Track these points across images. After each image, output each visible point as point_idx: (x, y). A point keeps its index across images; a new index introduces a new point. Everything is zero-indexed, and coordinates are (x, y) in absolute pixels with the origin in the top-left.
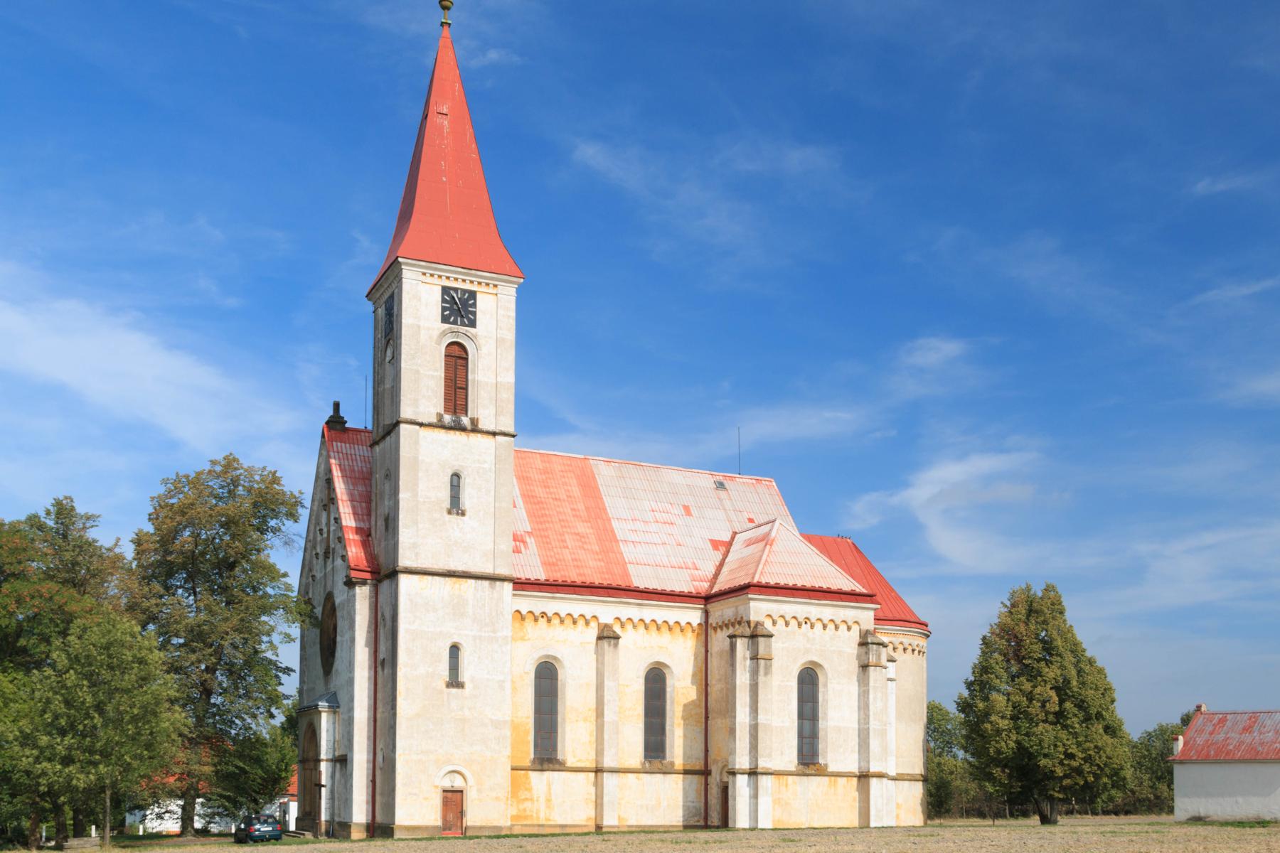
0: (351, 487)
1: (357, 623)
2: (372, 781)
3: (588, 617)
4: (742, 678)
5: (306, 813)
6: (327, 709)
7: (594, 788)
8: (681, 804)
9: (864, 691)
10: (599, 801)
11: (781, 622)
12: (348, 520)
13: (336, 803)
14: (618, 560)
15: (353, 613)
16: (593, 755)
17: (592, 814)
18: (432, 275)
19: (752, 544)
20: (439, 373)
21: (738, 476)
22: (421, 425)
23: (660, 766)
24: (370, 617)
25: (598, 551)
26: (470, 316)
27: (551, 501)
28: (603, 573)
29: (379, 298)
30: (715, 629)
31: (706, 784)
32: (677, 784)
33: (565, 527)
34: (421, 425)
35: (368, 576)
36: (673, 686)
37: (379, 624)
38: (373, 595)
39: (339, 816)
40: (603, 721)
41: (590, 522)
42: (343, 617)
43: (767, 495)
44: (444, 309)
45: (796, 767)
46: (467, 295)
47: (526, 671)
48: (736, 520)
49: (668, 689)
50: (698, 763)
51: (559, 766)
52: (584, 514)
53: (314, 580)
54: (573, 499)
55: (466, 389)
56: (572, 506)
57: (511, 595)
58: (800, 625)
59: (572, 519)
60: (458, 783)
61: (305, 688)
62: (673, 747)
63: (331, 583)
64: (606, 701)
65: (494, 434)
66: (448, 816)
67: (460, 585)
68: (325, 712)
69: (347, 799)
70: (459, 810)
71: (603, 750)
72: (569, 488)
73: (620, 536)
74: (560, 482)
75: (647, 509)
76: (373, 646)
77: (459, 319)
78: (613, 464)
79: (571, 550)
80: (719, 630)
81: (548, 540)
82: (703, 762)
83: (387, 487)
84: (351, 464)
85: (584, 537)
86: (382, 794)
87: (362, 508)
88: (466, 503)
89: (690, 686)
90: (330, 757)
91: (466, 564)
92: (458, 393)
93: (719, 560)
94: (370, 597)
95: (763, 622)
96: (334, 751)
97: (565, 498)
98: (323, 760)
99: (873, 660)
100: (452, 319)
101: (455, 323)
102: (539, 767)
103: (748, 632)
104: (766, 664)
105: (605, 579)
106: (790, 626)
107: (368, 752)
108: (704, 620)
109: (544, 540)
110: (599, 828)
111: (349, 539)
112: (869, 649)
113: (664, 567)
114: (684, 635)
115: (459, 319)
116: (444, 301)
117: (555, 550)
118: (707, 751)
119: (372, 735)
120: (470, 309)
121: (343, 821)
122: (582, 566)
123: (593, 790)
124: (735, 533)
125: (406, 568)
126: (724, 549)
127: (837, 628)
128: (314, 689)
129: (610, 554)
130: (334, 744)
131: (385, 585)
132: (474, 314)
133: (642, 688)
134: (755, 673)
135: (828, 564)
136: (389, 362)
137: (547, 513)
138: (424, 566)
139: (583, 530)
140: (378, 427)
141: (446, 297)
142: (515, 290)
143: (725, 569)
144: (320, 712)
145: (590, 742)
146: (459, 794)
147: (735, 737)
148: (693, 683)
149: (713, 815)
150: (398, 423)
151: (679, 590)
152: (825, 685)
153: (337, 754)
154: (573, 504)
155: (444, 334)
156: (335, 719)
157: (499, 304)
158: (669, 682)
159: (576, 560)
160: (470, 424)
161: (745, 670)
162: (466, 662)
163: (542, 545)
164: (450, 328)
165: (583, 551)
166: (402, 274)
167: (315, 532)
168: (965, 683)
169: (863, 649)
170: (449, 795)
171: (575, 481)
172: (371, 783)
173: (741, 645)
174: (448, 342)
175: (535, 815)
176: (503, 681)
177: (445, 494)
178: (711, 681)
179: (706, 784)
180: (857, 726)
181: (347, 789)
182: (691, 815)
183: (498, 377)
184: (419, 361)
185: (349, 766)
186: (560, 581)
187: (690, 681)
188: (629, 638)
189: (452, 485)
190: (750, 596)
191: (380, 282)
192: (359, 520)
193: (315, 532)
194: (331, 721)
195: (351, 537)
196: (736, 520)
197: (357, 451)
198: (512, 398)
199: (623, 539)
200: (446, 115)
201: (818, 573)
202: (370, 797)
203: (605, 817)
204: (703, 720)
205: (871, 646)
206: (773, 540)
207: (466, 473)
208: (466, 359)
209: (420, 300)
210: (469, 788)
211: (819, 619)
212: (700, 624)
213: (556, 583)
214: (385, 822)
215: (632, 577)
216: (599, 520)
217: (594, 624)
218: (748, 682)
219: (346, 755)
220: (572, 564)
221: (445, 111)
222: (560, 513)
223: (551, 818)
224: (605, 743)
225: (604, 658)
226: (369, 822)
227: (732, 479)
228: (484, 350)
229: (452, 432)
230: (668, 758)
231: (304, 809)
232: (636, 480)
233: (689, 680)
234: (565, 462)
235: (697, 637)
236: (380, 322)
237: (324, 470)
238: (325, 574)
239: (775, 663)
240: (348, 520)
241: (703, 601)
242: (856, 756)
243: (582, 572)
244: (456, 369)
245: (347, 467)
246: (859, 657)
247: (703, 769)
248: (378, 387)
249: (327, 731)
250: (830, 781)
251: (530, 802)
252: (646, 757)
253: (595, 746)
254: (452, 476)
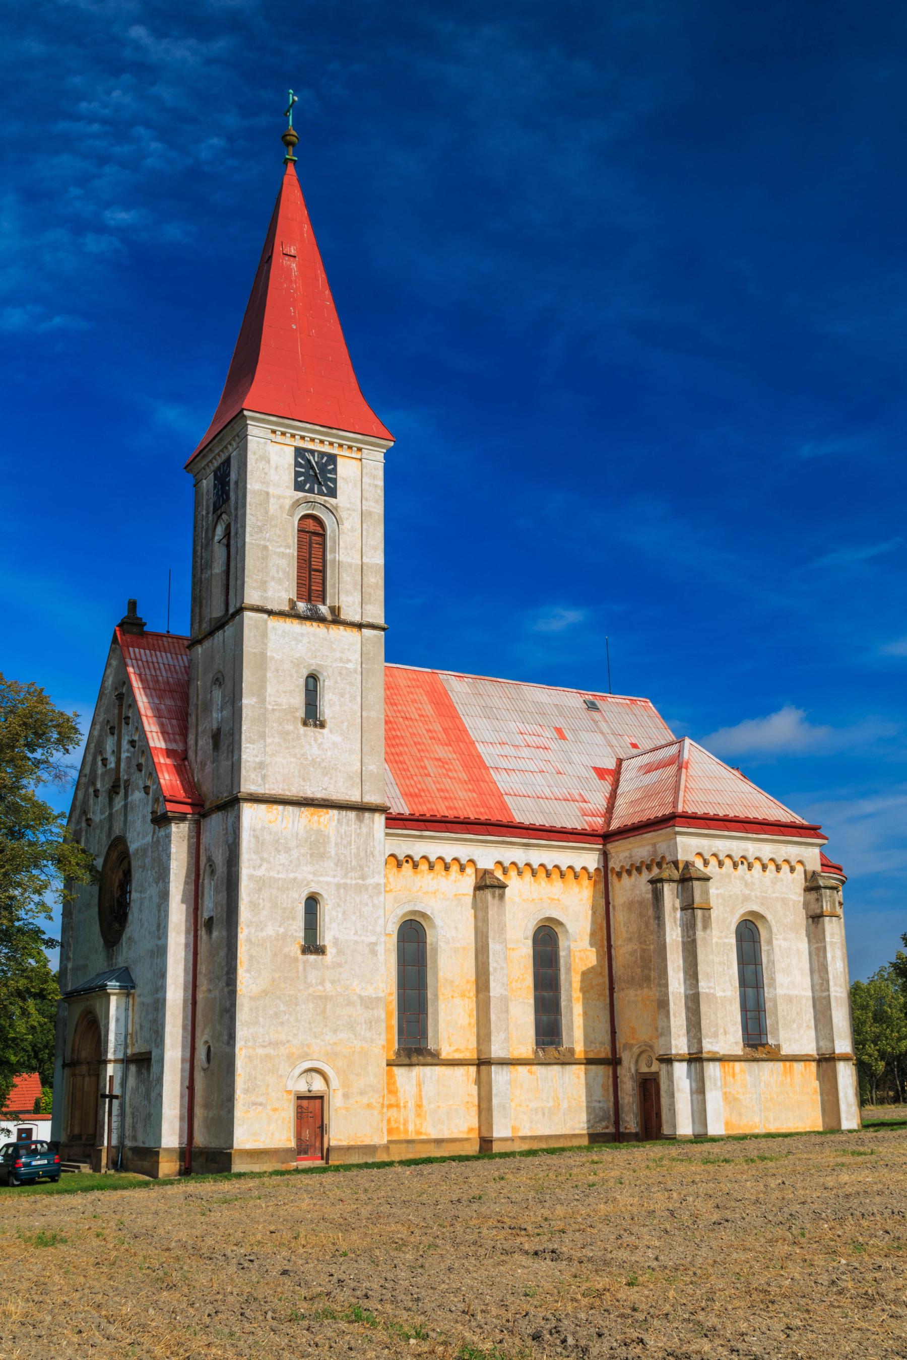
0: (157, 701)
1: (172, 871)
2: (188, 1088)
3: (463, 861)
4: (673, 935)
5: (73, 1136)
6: (117, 991)
7: (476, 1087)
8: (585, 1104)
9: (818, 949)
10: (484, 1105)
11: (713, 862)
12: (156, 741)
13: (128, 1121)
14: (492, 792)
15: (164, 858)
16: (473, 1044)
17: (475, 1123)
18: (283, 434)
19: (656, 769)
20: (291, 551)
21: (609, 695)
22: (270, 613)
23: (556, 1055)
24: (188, 865)
25: (466, 779)
26: (329, 483)
27: (401, 720)
28: (477, 806)
29: (204, 468)
30: (619, 875)
31: (615, 1077)
32: (578, 1077)
33: (423, 751)
34: (270, 613)
35: (187, 809)
36: (569, 950)
37: (201, 872)
38: (194, 834)
39: (134, 1138)
40: (489, 997)
41: (451, 745)
42: (143, 867)
43: (645, 717)
44: (297, 474)
45: (743, 1050)
46: (325, 458)
47: (387, 932)
48: (618, 745)
49: (562, 953)
50: (602, 1050)
51: (433, 1059)
52: (442, 736)
53: (89, 825)
54: (427, 719)
55: (323, 571)
56: (426, 727)
57: (382, 835)
58: (735, 866)
59: (429, 741)
60: (318, 1085)
61: (70, 966)
62: (572, 1029)
63: (122, 825)
64: (491, 969)
65: (360, 626)
66: (303, 1134)
67: (320, 816)
68: (115, 994)
69: (149, 1116)
70: (318, 1124)
71: (489, 1035)
72: (420, 706)
73: (488, 762)
74: (409, 700)
75: (515, 732)
76: (193, 902)
77: (316, 487)
78: (465, 679)
79: (434, 779)
80: (625, 875)
81: (405, 766)
82: (609, 1048)
83: (217, 695)
84: (154, 674)
85: (447, 763)
86: (207, 1106)
87: (172, 726)
88: (326, 711)
89: (589, 948)
90: (120, 1056)
91: (326, 789)
92: (313, 577)
93: (609, 791)
94: (189, 836)
95: (694, 862)
96: (126, 1047)
97: (417, 717)
98: (110, 1061)
99: (827, 908)
100: (308, 485)
101: (311, 491)
102: (406, 1061)
103: (676, 875)
104: (704, 916)
105: (481, 813)
106: (724, 868)
107: (184, 1047)
108: (602, 864)
109: (400, 766)
110: (486, 1143)
111: (160, 763)
112: (821, 895)
113: (547, 798)
114: (579, 884)
115: (316, 487)
116: (297, 464)
117: (415, 778)
118: (613, 1032)
119: (189, 1023)
120: (329, 475)
121: (142, 1145)
122: (451, 798)
123: (474, 1090)
124: (620, 762)
125: (251, 795)
126: (612, 779)
127: (778, 868)
128: (86, 966)
129: (482, 784)
130: (126, 1038)
131: (215, 821)
132: (334, 481)
133: (530, 951)
134: (689, 928)
135: (756, 792)
136: (219, 542)
137: (399, 734)
138: (273, 792)
139: (445, 755)
140: (200, 622)
141: (300, 460)
142: (383, 454)
143: (620, 802)
144: (108, 996)
145: (470, 1024)
146: (318, 1101)
147: (668, 1012)
148: (592, 945)
149: (627, 1119)
150: (240, 610)
151: (570, 827)
152: (770, 942)
153: (129, 1052)
154: (427, 724)
155: (297, 504)
156: (127, 1003)
157: (365, 471)
158: (563, 943)
159: (442, 790)
160: (330, 614)
161: (676, 924)
162: (327, 919)
163: (398, 772)
164: (306, 497)
165: (449, 780)
166: (247, 430)
167: (94, 763)
168: (904, 939)
169: (813, 896)
170: (305, 1103)
171: (425, 698)
172: (187, 1090)
173: (669, 892)
174: (302, 514)
175: (402, 1127)
176: (375, 944)
177: (298, 700)
178: (617, 941)
179: (615, 1077)
180: (810, 994)
181: (149, 1100)
182: (597, 1119)
183: (364, 558)
184: (268, 535)
185: (154, 1069)
186: (428, 815)
187: (588, 942)
188: (515, 886)
189: (307, 690)
190: (677, 829)
191: (211, 446)
192: (170, 740)
193: (94, 763)
194: (123, 1006)
195: (162, 761)
196: (618, 745)
197: (160, 658)
198: (381, 583)
199: (493, 766)
200: (295, 257)
201: (748, 802)
202: (186, 1110)
203: (495, 1127)
204: (607, 992)
205: (823, 890)
206: (687, 763)
207: (325, 674)
208: (323, 536)
209: (269, 462)
210: (331, 1091)
211: (757, 859)
212: (597, 870)
213: (424, 818)
214: (213, 1145)
215: (513, 811)
216: (461, 744)
217: (470, 871)
218: (680, 939)
219: (150, 1053)
220: (438, 795)
221: (293, 252)
222: (414, 734)
223: (423, 1130)
224: (493, 1026)
225: (487, 913)
226: (184, 1146)
227: (603, 699)
228: (346, 526)
229: (308, 623)
230: (566, 1045)
231: (71, 1131)
232: (495, 698)
233: (587, 939)
234: (410, 676)
235: (595, 886)
236: (205, 497)
237: (112, 685)
238: (111, 815)
239: (714, 914)
240: (156, 741)
241: (600, 840)
242: (812, 1033)
243: (451, 804)
244: (310, 546)
245: (149, 677)
246: (806, 905)
247: (610, 1056)
248: (201, 573)
249: (117, 1020)
250: (785, 1067)
251: (395, 1109)
252: (538, 1043)
253: (475, 1030)
254: (307, 677)
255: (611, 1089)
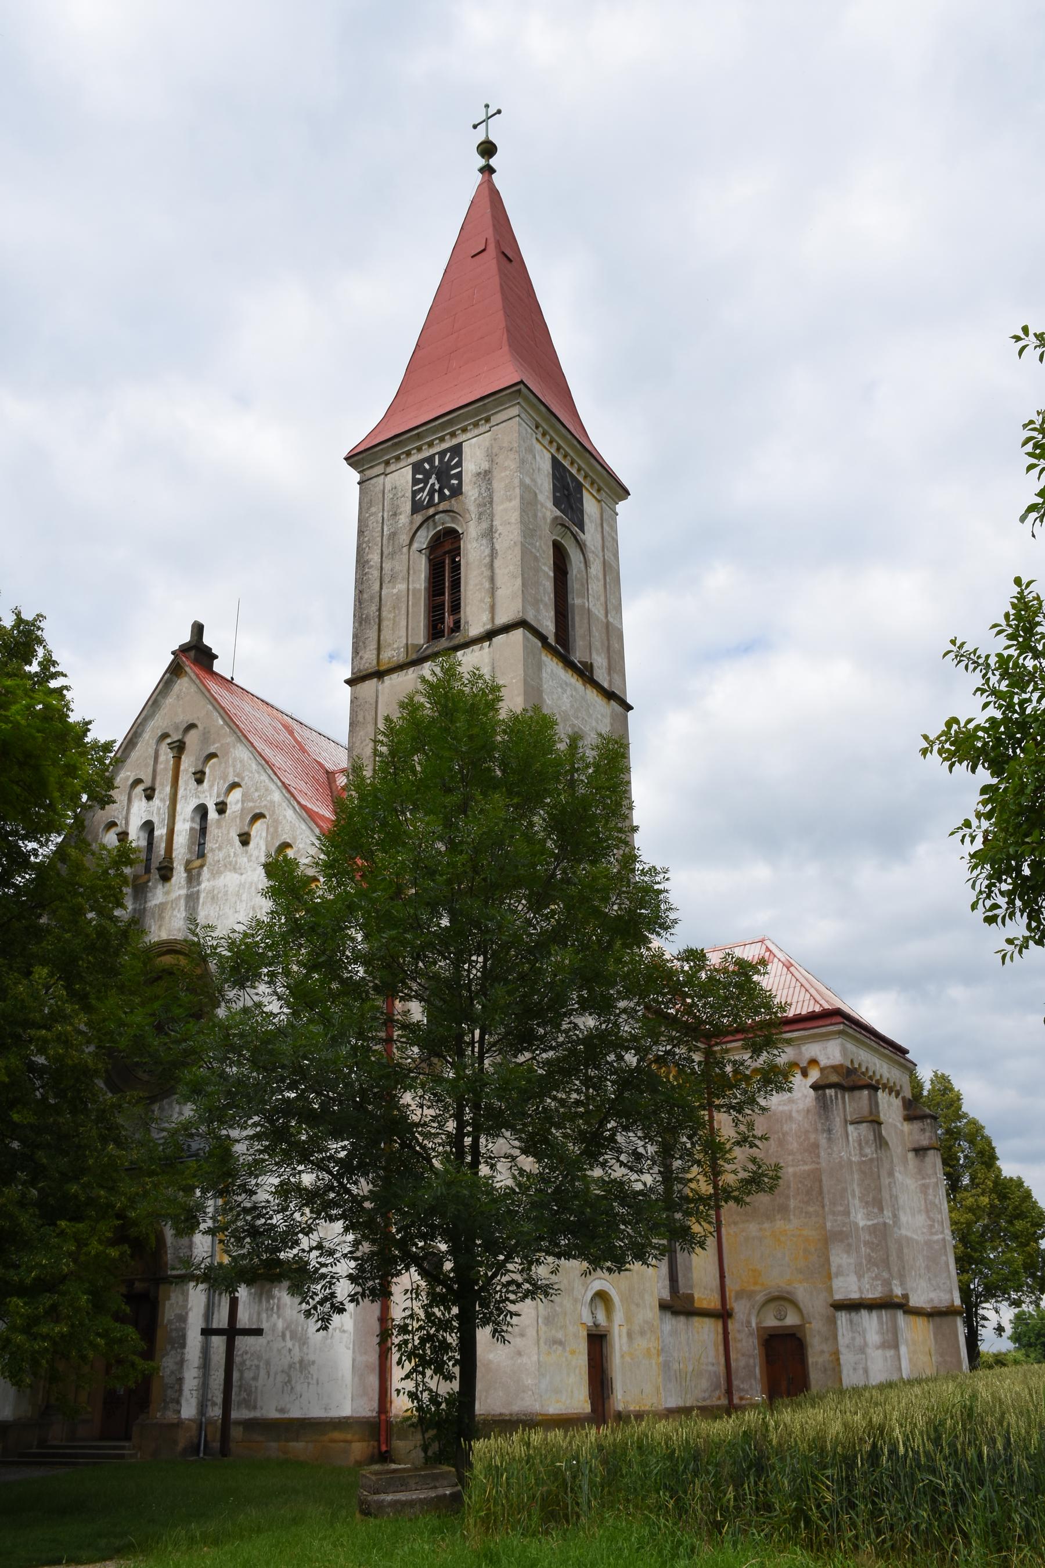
118: (722, 1277)
255: (721, 1348)
